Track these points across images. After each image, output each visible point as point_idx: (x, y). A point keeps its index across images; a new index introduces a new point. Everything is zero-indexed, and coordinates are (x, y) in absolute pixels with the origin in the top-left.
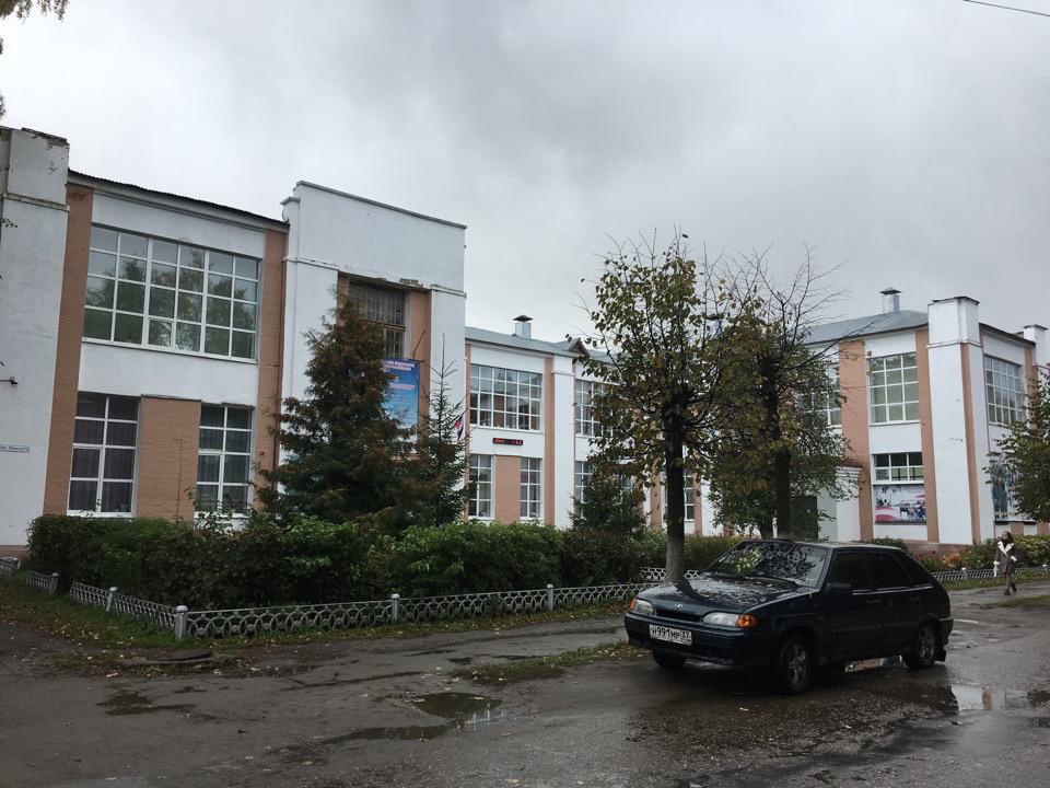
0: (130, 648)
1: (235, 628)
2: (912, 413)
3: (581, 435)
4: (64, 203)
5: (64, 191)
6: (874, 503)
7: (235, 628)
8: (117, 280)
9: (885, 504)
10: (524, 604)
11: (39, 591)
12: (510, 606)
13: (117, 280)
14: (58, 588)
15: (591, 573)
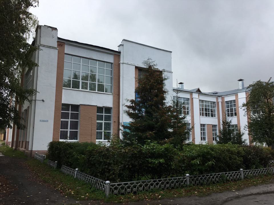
0: (87, 199)
1: (129, 190)
3: (201, 116)
4: (56, 47)
5: (56, 44)
7: (129, 190)
8: (72, 79)
10: (233, 177)
11: (51, 167)
12: (228, 178)
13: (72, 79)
14: (57, 166)
15: (254, 164)
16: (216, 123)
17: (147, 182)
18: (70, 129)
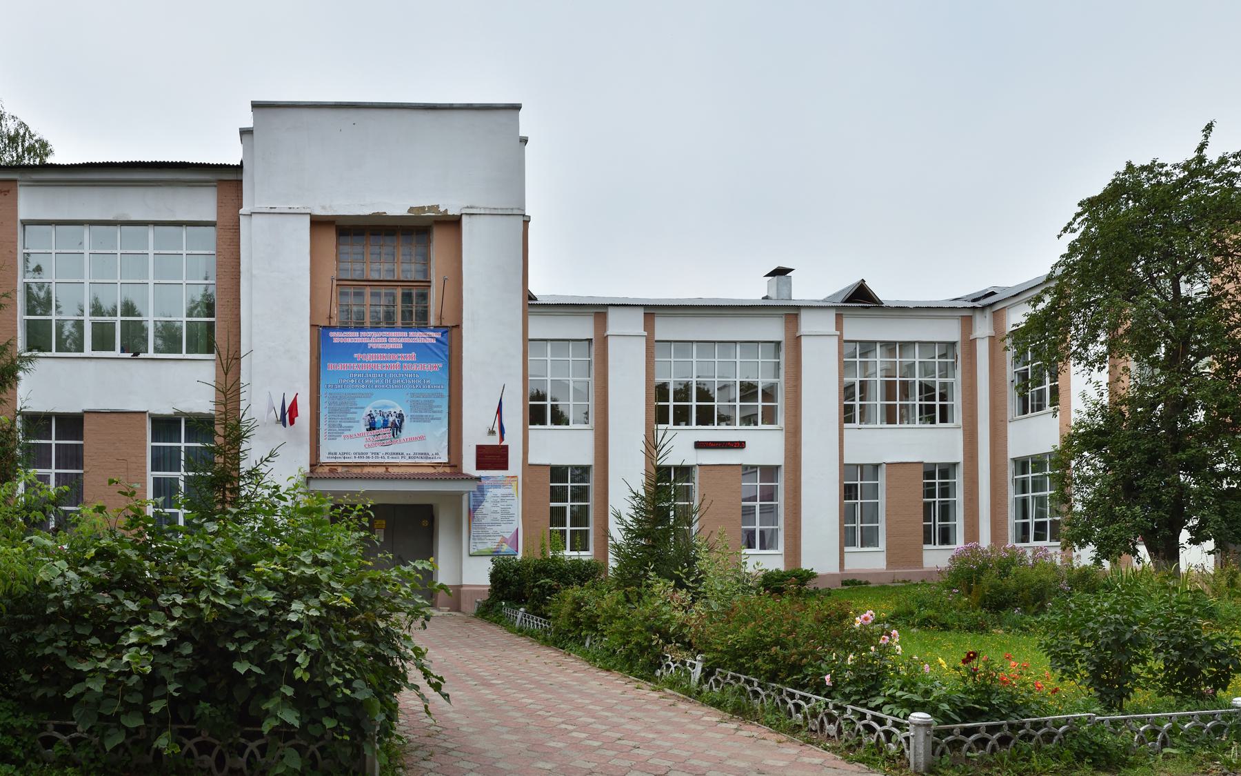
17: (1028, 726)
18: (760, 525)
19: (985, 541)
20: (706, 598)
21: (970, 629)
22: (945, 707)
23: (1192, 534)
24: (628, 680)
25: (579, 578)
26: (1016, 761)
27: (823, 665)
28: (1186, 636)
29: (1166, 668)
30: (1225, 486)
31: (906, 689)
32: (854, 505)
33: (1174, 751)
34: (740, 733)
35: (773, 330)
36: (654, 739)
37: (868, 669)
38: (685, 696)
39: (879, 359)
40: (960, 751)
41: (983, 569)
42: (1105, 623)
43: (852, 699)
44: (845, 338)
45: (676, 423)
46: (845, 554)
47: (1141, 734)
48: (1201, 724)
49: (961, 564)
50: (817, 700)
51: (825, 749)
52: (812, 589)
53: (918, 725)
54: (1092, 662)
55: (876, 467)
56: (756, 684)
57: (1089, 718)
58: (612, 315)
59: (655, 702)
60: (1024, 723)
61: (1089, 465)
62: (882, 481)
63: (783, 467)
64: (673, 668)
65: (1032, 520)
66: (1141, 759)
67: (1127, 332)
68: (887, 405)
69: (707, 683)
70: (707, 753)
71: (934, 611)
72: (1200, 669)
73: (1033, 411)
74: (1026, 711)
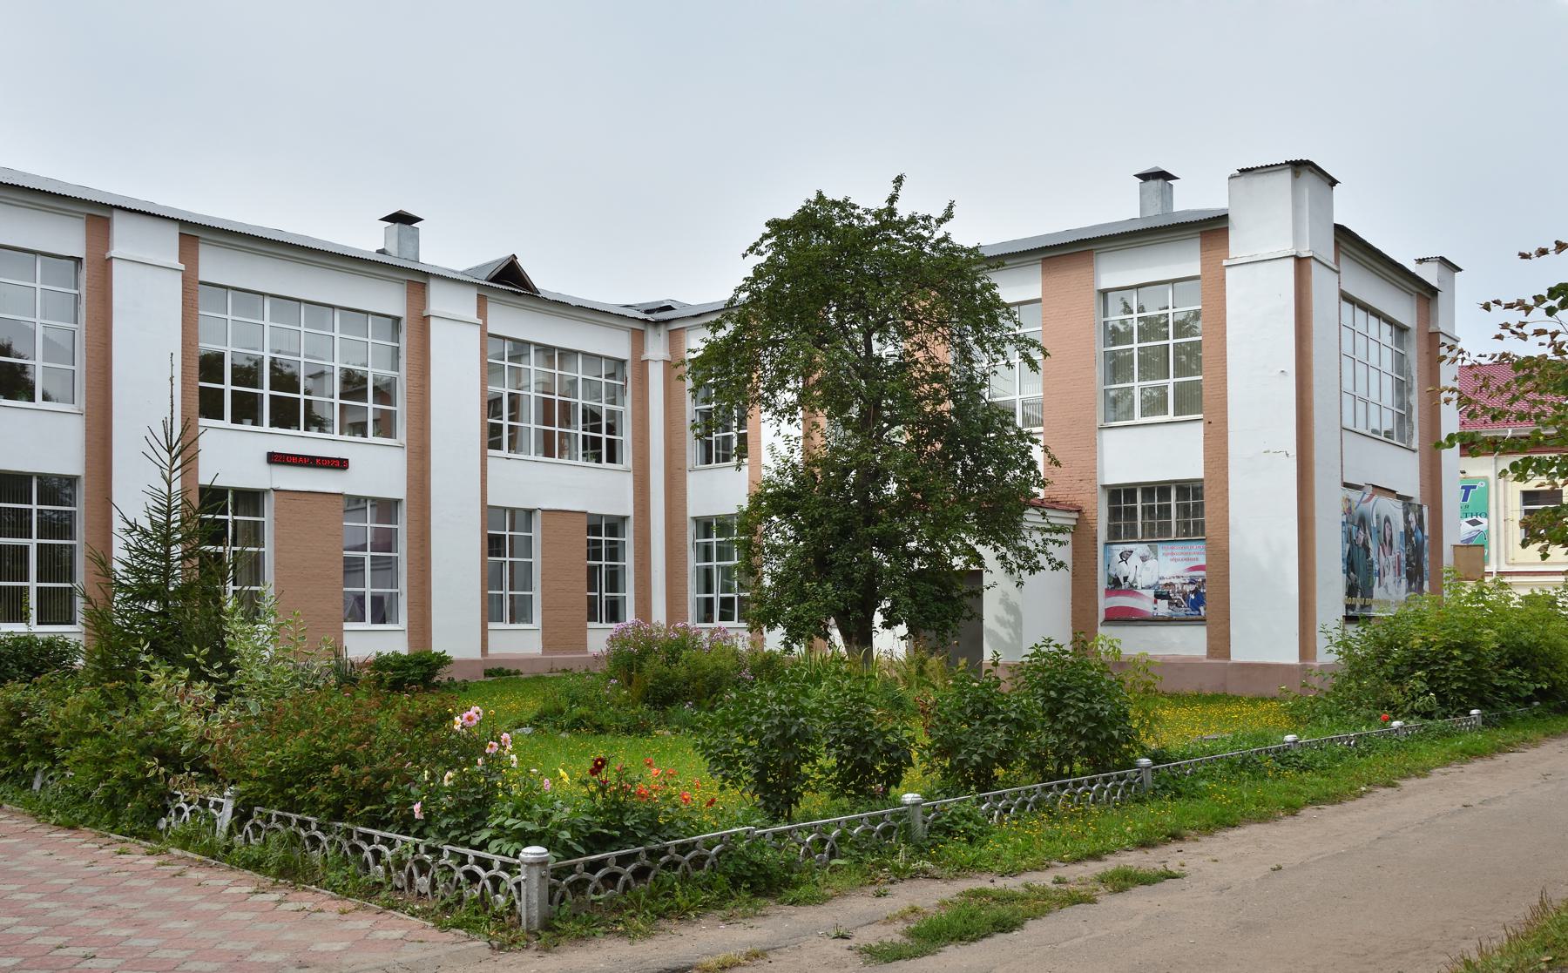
2: (1188, 401)
6: (1102, 584)
9: (1125, 586)
16: (623, 505)
17: (672, 851)
19: (659, 614)
20: (241, 695)
21: (628, 731)
22: (566, 834)
23: (885, 617)
24: (106, 840)
25: (29, 668)
26: (657, 900)
27: (413, 790)
28: (855, 728)
29: (840, 765)
30: (916, 566)
31: (518, 815)
32: (502, 563)
33: (842, 862)
34: (284, 906)
35: (390, 300)
36: (128, 937)
37: (472, 790)
38: (203, 858)
39: (533, 366)
40: (584, 894)
41: (645, 653)
42: (769, 716)
43: (450, 836)
44: (490, 331)
45: (236, 419)
46: (489, 633)
47: (807, 846)
48: (870, 827)
49: (900, 357)
50: (404, 842)
51: (413, 915)
52: (445, 680)
53: (531, 864)
54: (757, 765)
55: (530, 513)
56: (314, 826)
57: (748, 832)
58: (120, 224)
59: (147, 874)
60: (667, 848)
61: (778, 532)
62: (536, 534)
63: (405, 503)
64: (187, 814)
65: (717, 596)
66: (805, 876)
67: (818, 382)
68: (616, 592)
69: (241, 832)
70: (220, 947)
71: (587, 708)
72: (873, 764)
73: (717, 461)
74: (670, 832)
